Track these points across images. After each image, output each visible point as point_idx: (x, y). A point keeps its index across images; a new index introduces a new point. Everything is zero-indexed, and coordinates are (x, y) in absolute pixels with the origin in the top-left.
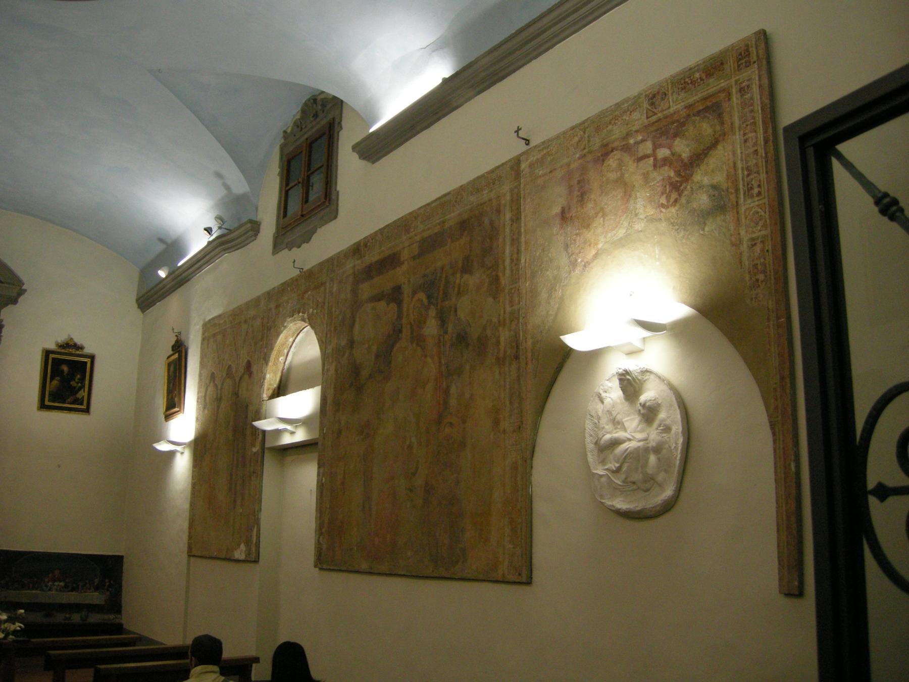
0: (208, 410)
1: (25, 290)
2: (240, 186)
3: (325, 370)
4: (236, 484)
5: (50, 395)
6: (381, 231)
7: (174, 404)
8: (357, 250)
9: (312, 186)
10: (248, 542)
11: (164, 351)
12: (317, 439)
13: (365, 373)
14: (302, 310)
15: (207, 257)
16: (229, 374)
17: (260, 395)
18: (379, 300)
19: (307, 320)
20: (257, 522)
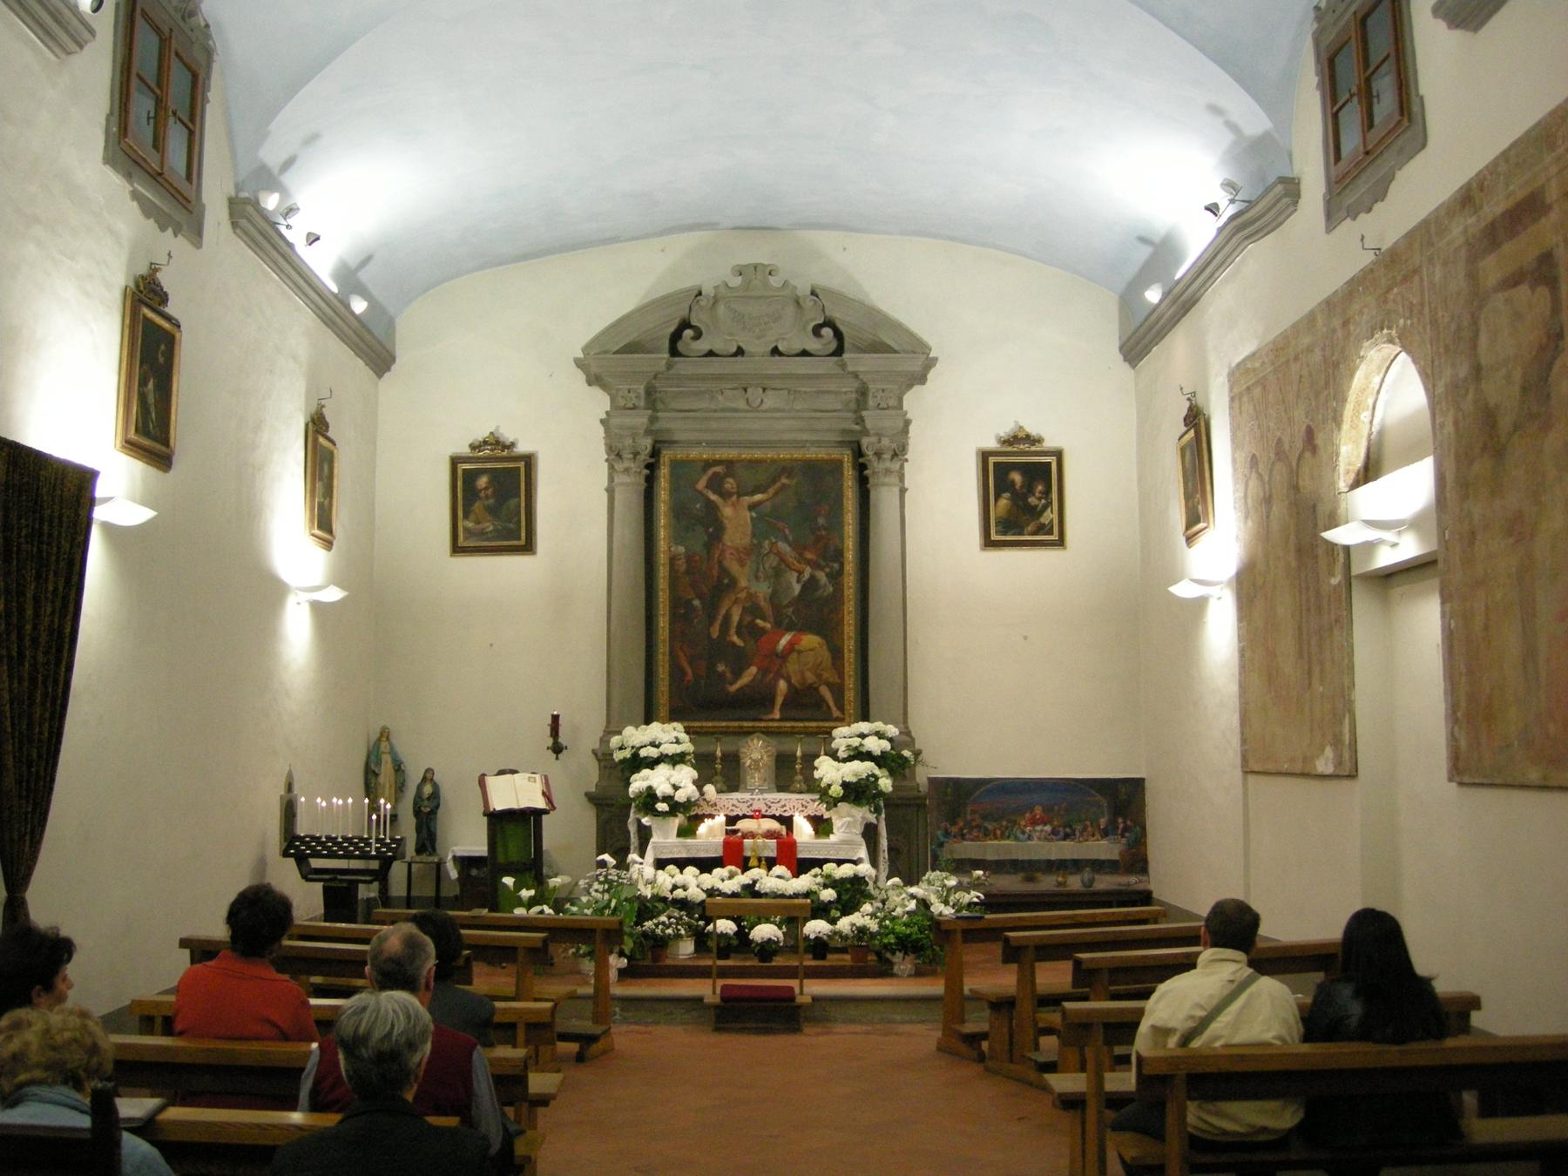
0: (1253, 521)
1: (936, 359)
2: (1255, 121)
3: (1437, 427)
4: (1309, 645)
5: (997, 523)
6: (1504, 155)
7: (1196, 515)
8: (1467, 198)
9: (1378, 96)
10: (1337, 742)
11: (1173, 426)
12: (1435, 552)
13: (1505, 423)
14: (1386, 323)
15: (1219, 257)
16: (1280, 454)
17: (1333, 484)
18: (1516, 284)
19: (1397, 340)
20: (1349, 707)
